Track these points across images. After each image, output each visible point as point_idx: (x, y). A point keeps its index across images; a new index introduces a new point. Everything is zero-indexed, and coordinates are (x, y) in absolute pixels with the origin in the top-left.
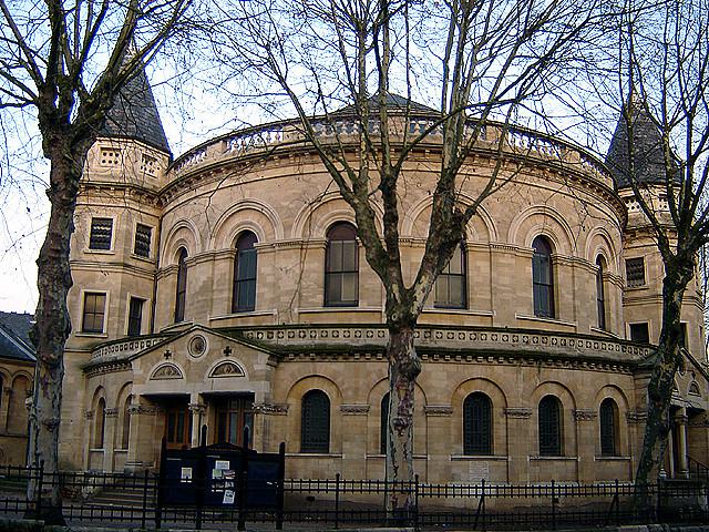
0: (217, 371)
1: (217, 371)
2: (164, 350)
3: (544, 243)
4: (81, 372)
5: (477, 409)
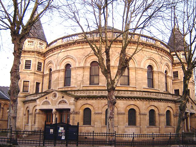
0: (60, 103)
1: (60, 103)
2: (45, 97)
3: (150, 67)
4: (22, 103)
5: (132, 113)
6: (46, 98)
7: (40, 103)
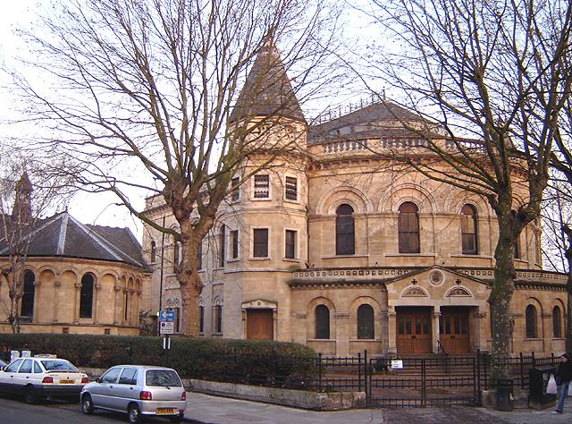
0: (452, 294)
1: (452, 294)
2: (411, 279)
3: (345, 209)
4: (287, 286)
5: (365, 313)
6: (414, 282)
7: (399, 292)
